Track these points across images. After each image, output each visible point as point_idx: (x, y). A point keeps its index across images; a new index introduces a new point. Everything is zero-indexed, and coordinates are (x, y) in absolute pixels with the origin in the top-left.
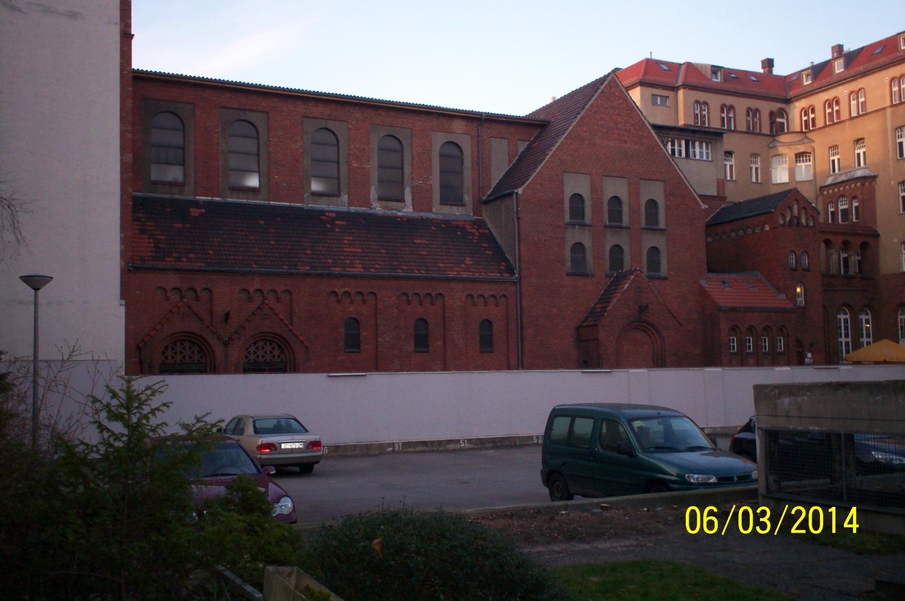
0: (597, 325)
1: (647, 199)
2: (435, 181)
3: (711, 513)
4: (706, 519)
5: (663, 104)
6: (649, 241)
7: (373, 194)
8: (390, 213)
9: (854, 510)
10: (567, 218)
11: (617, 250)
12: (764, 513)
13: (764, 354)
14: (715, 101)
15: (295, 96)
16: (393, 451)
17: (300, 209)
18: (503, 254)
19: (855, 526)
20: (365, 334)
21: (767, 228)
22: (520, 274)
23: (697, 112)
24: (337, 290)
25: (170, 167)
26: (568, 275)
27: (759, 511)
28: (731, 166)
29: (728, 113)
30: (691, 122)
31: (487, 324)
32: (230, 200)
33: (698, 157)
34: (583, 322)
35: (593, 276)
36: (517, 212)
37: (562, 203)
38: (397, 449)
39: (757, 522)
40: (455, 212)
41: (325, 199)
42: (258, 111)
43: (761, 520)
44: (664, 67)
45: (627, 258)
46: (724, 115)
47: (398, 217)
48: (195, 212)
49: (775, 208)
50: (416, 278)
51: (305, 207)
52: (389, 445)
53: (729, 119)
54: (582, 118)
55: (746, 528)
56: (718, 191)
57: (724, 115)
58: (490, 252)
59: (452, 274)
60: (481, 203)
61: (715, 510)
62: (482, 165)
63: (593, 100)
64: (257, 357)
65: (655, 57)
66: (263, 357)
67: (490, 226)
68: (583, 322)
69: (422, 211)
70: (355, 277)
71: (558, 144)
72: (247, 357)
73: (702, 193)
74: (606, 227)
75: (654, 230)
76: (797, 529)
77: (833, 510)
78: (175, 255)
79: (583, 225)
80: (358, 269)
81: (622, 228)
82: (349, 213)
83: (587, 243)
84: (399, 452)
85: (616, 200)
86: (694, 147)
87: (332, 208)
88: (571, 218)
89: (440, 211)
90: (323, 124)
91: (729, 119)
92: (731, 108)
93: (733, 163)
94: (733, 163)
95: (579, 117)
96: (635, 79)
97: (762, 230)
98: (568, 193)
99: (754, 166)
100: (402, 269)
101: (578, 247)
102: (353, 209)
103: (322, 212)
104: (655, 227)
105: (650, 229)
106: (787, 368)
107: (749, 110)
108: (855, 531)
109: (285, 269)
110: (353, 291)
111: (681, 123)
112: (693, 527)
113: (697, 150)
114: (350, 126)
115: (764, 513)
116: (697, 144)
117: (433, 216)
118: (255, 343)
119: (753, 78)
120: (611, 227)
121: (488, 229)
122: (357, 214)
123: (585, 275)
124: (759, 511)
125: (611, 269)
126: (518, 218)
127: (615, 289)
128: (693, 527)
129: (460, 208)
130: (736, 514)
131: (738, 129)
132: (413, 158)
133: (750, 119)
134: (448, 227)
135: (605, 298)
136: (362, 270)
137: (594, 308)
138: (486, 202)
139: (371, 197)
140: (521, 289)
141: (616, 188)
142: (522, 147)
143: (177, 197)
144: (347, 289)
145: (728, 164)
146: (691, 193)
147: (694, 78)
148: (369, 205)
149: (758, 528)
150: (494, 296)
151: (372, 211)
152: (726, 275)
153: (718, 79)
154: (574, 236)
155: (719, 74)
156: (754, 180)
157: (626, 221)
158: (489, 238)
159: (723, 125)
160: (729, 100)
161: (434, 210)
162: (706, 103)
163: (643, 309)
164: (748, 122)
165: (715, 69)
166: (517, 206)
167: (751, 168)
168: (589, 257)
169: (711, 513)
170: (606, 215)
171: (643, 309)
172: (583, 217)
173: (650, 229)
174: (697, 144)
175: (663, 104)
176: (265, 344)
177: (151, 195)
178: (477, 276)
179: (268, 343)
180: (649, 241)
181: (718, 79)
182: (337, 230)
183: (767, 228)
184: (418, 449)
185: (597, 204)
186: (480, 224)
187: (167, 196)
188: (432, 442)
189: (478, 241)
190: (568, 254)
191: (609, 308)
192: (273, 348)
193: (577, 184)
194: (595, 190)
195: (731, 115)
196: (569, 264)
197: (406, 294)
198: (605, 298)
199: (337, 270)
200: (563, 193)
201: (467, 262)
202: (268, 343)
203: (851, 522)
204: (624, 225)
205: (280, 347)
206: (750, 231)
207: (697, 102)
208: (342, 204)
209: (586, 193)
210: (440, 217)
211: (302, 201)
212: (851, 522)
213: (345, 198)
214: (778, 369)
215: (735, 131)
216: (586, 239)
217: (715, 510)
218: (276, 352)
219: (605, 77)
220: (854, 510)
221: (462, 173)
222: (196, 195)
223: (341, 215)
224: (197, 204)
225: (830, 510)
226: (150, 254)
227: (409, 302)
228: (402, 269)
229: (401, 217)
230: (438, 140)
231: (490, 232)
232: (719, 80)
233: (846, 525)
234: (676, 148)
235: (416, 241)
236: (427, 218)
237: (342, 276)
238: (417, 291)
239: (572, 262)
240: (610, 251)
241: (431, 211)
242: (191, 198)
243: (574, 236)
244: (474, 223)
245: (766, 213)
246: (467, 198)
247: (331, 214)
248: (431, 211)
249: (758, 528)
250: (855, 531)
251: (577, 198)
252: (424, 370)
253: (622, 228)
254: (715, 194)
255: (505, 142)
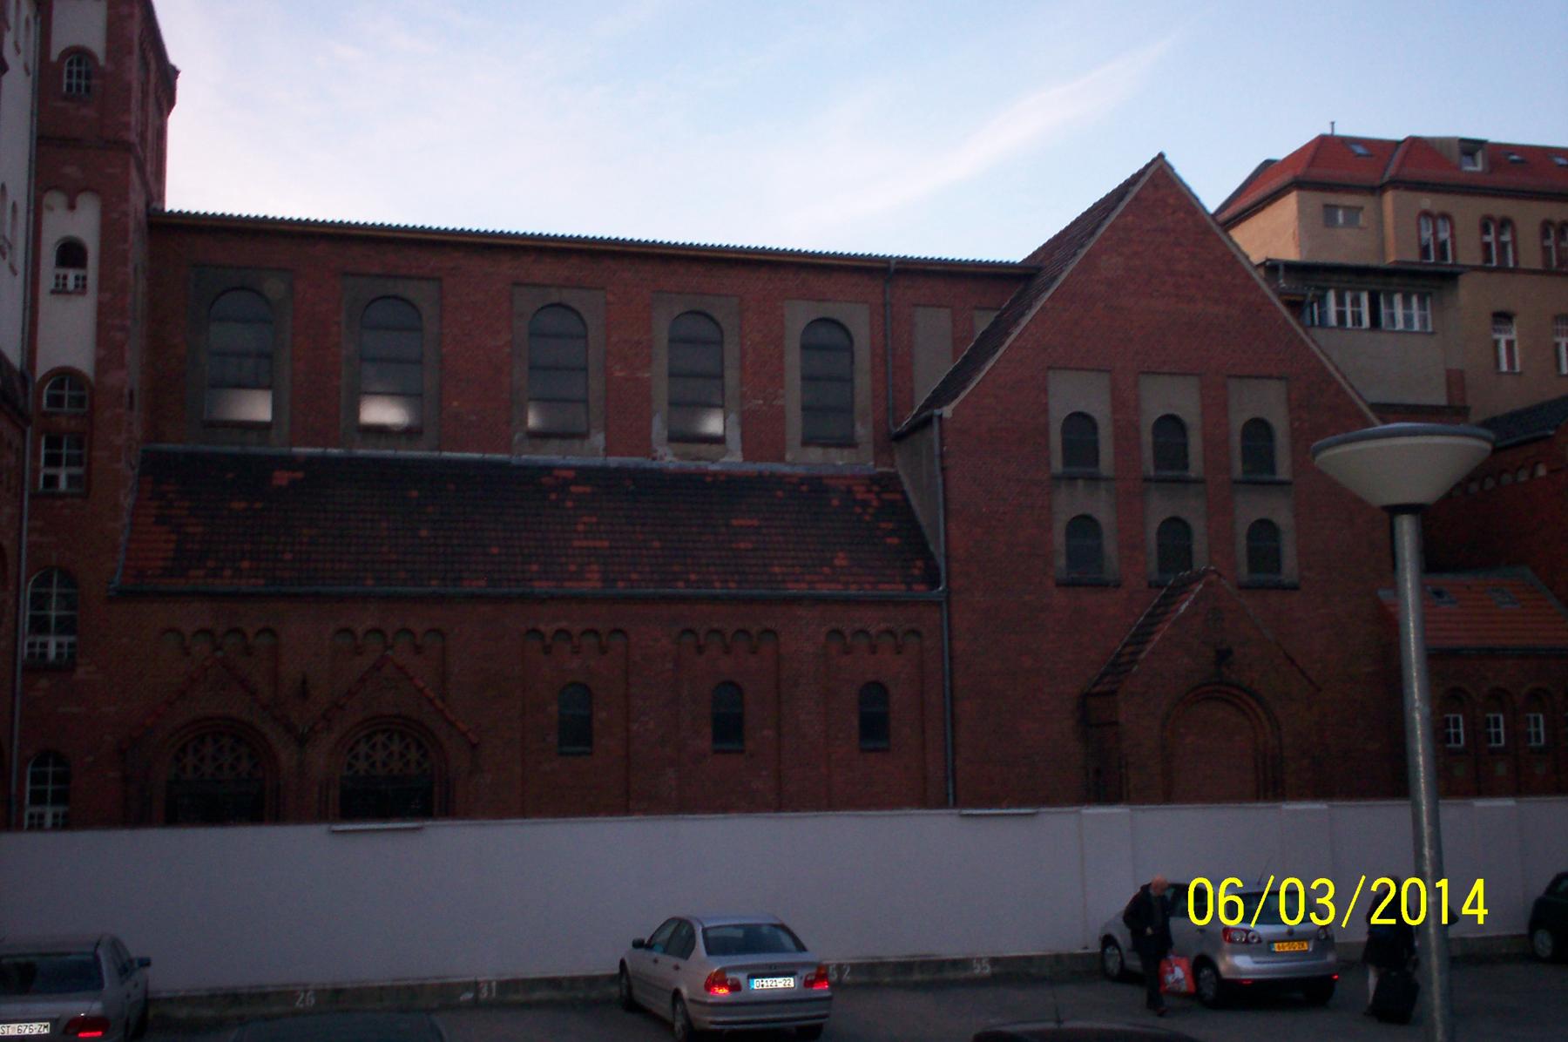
0: (1113, 692)
1: (1247, 416)
2: (792, 397)
3: (1231, 888)
4: (1222, 901)
5: (1351, 221)
6: (1250, 509)
7: (658, 429)
8: (690, 465)
9: (1479, 885)
10: (1057, 465)
11: (1175, 528)
12: (1323, 890)
13: (1492, 752)
14: (1469, 211)
15: (792, 264)
16: (476, 1000)
17: (498, 465)
18: (925, 545)
19: (1481, 912)
20: (603, 715)
21: (1541, 471)
22: (948, 585)
23: (1427, 235)
24: (542, 627)
25: (244, 392)
26: (1060, 584)
27: (1314, 886)
28: (1510, 344)
29: (1499, 233)
30: (1413, 256)
31: (875, 692)
32: (361, 452)
33: (1400, 326)
34: (1095, 685)
35: (1118, 586)
36: (942, 456)
37: (1044, 432)
38: (484, 994)
39: (1311, 906)
40: (840, 460)
41: (555, 443)
42: (421, 278)
43: (1319, 901)
44: (1360, 150)
45: (1200, 546)
46: (1490, 238)
47: (705, 474)
48: (282, 478)
49: (1557, 427)
50: (715, 599)
51: (515, 460)
52: (467, 986)
53: (1502, 247)
54: (1088, 255)
55: (1292, 915)
56: (1450, 395)
57: (1490, 238)
58: (895, 541)
59: (794, 589)
60: (893, 439)
61: (1239, 884)
62: (894, 361)
63: (1113, 217)
64: (373, 765)
65: (1341, 131)
66: (384, 764)
67: (907, 486)
68: (1095, 685)
69: (762, 459)
70: (582, 599)
71: (1034, 311)
72: (350, 766)
73: (1375, 400)
74: (1147, 480)
75: (1263, 483)
76: (1380, 917)
77: (1443, 884)
78: (210, 564)
79: (1094, 479)
80: (592, 584)
81: (1186, 481)
82: (603, 471)
83: (1104, 514)
84: (490, 1005)
85: (1171, 426)
86: (1390, 304)
87: (573, 460)
88: (1067, 462)
89: (801, 460)
90: (555, 296)
91: (1502, 247)
92: (1505, 223)
93: (1514, 336)
94: (1514, 336)
95: (1083, 252)
96: (1286, 178)
97: (1532, 475)
98: (1238, 421)
99: (1503, 339)
100: (687, 581)
101: (1083, 526)
102: (614, 461)
103: (548, 469)
104: (1266, 477)
105: (1255, 483)
106: (1510, 802)
107: (1546, 226)
108: (1481, 921)
109: (435, 586)
110: (547, 629)
111: (1391, 258)
112: (1201, 913)
113: (1399, 312)
114: (611, 298)
115: (1323, 890)
116: (1398, 298)
117: (786, 469)
118: (369, 737)
119: (1561, 161)
120: (1164, 480)
121: (903, 492)
122: (621, 471)
123: (1101, 585)
124: (1314, 886)
125: (1163, 568)
126: (943, 469)
127: (1164, 613)
128: (1201, 913)
129: (846, 452)
130: (1274, 893)
131: (1523, 265)
132: (743, 355)
133: (1550, 242)
134: (815, 487)
135: (1142, 635)
136: (599, 585)
137: (1119, 655)
138: (899, 437)
139: (654, 436)
140: (949, 618)
141: (1174, 396)
142: (983, 322)
143: (253, 449)
144: (563, 624)
145: (1503, 339)
146: (1352, 403)
147: (1420, 167)
148: (649, 452)
149: (1313, 916)
150: (890, 632)
151: (655, 465)
152: (1448, 577)
153: (1477, 166)
154: (1068, 504)
155: (1479, 156)
156: (1504, 367)
157: (1196, 467)
158: (902, 513)
159: (1488, 259)
160: (1499, 207)
161: (788, 457)
162: (1445, 216)
163: (1223, 656)
164: (1546, 250)
165: (1471, 147)
166: (942, 445)
167: (1497, 342)
168: (1110, 546)
169: (1231, 888)
170: (1148, 453)
171: (1223, 656)
172: (1096, 462)
173: (1255, 483)
174: (1398, 298)
175: (1351, 221)
176: (390, 738)
177: (203, 448)
178: (853, 591)
179: (396, 737)
180: (1250, 509)
181: (1477, 166)
182: (569, 504)
183: (1541, 471)
184: (538, 995)
185: (1126, 434)
186: (887, 483)
187: (236, 449)
188: (573, 980)
189: (884, 521)
190: (1059, 538)
191: (1143, 655)
192: (407, 747)
193: (1074, 394)
194: (1123, 405)
195: (1506, 238)
196: (1061, 562)
197: (691, 631)
198: (1142, 635)
199: (542, 587)
200: (1045, 410)
201: (837, 562)
202: (396, 737)
203: (1474, 905)
204: (1192, 474)
205: (420, 746)
206: (1506, 478)
207: (1426, 214)
208: (593, 452)
209: (1100, 410)
210: (800, 470)
211: (508, 448)
212: (1474, 905)
213: (598, 439)
214: (1480, 803)
215: (1516, 270)
216: (1102, 508)
217: (1239, 884)
218: (413, 755)
219: (1141, 173)
220: (1479, 885)
221: (851, 380)
222: (292, 445)
223: (585, 474)
224: (289, 462)
225: (1438, 885)
226: (161, 564)
227: (700, 650)
228: (687, 581)
229: (715, 474)
230: (798, 316)
231: (906, 500)
232: (1479, 168)
233: (1466, 911)
234: (1348, 310)
235: (734, 522)
236: (772, 475)
237: (552, 598)
238: (716, 626)
239: (1069, 558)
240: (1159, 533)
241: (781, 459)
242: (284, 450)
243: (1068, 504)
244: (874, 480)
245: (1536, 440)
246: (863, 431)
247: (564, 473)
248: (781, 459)
249: (1313, 916)
250: (1481, 921)
251: (1080, 424)
252: (565, 816)
253: (1186, 481)
254: (1443, 401)
255: (945, 314)
